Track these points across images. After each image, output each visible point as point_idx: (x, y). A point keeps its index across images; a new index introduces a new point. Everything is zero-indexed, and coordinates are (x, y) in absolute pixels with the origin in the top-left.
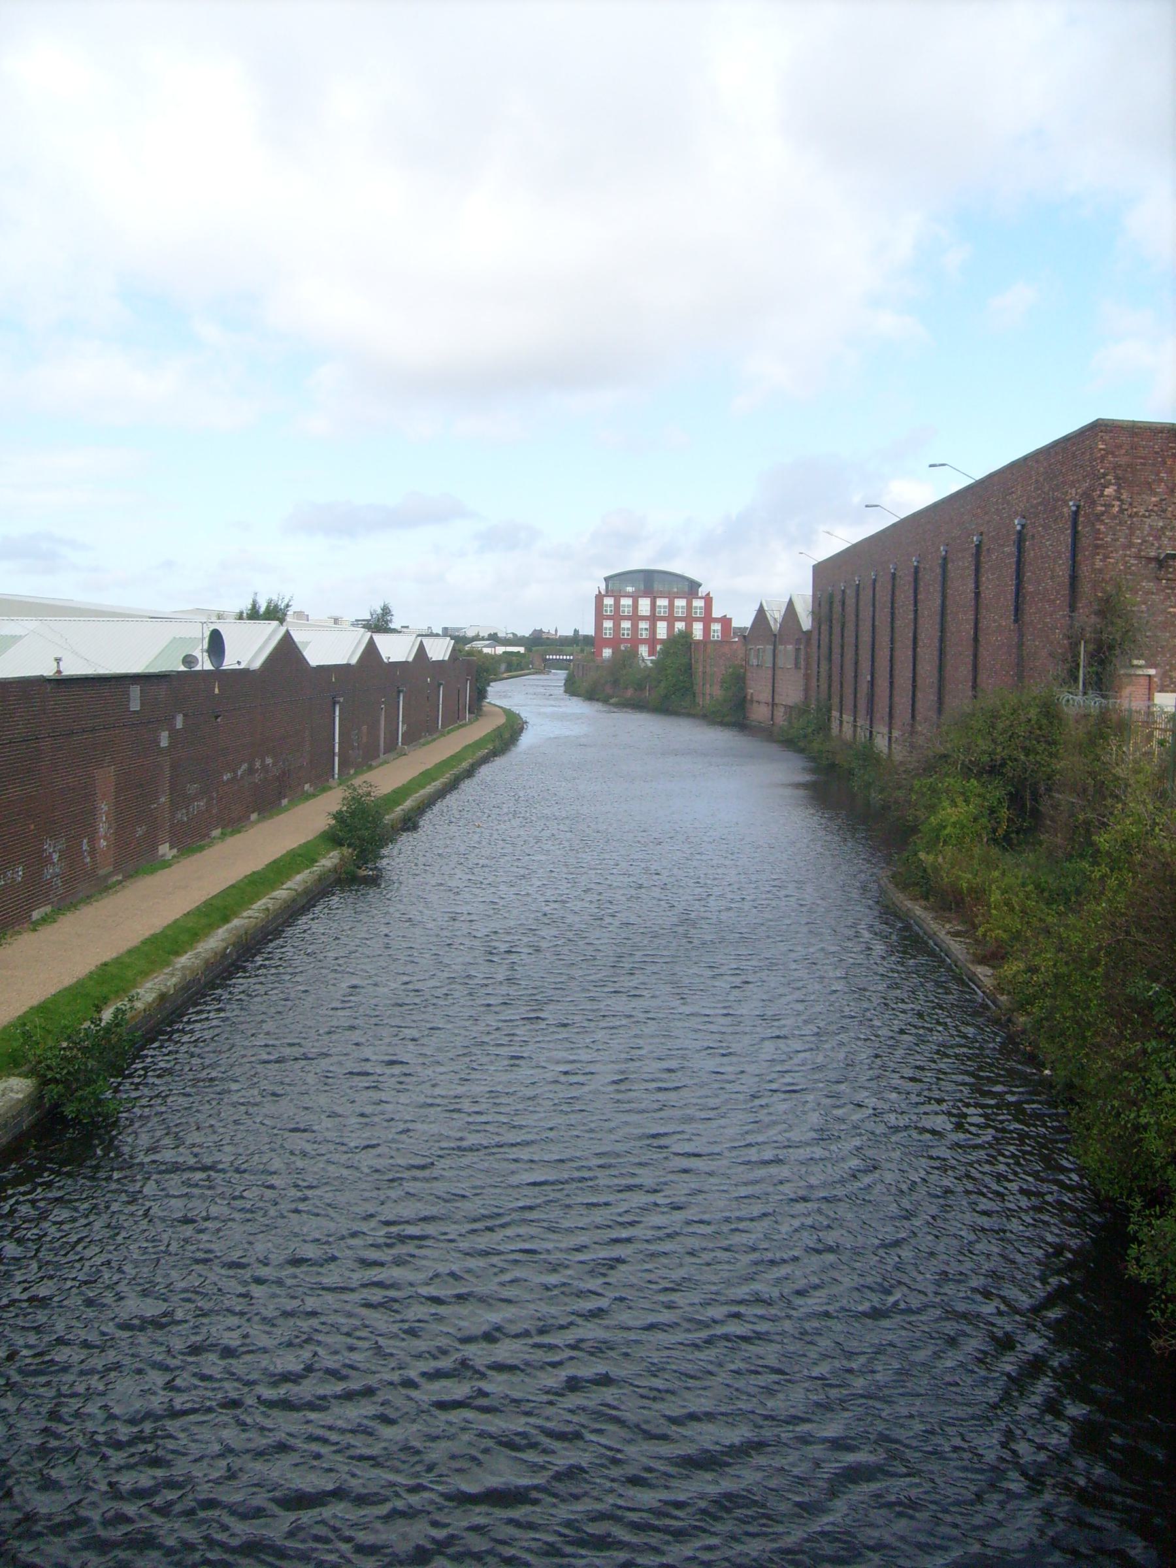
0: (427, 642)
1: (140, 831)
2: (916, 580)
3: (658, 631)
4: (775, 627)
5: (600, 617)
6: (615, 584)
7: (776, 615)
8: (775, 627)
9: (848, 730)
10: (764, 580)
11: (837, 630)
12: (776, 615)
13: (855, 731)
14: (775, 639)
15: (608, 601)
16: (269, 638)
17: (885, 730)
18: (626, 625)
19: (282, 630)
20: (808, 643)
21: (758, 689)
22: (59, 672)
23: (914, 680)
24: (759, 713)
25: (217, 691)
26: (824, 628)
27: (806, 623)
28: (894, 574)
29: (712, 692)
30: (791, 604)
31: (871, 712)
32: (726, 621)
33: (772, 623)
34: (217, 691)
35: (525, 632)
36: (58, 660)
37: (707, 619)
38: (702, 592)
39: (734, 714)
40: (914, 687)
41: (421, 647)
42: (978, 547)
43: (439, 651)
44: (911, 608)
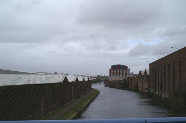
1: (47, 109)
4: (143, 74)
7: (143, 72)
8: (143, 74)
9: (157, 93)
10: (138, 66)
11: (154, 75)
12: (143, 72)
13: (158, 93)
14: (143, 76)
16: (63, 78)
17: (164, 92)
20: (149, 77)
21: (140, 85)
22: (29, 83)
24: (140, 89)
26: (152, 75)
27: (148, 74)
29: (133, 86)
30: (145, 70)
31: (161, 89)
33: (142, 74)
35: (96, 76)
36: (29, 81)
39: (136, 90)
41: (66, 78)
42: (180, 61)
43: (71, 79)
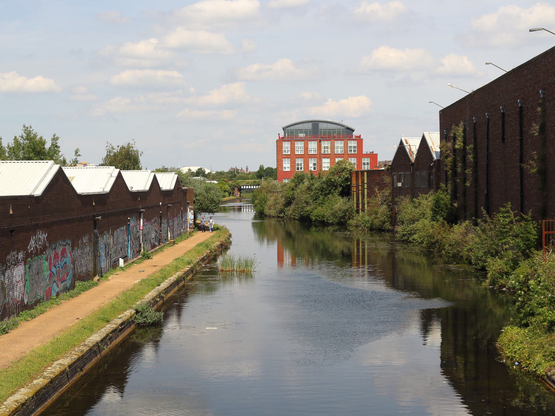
0: (159, 176)
2: (521, 116)
3: (324, 165)
5: (280, 156)
6: (290, 134)
15: (286, 146)
18: (300, 161)
19: (56, 167)
23: (522, 191)
25: (11, 212)
28: (503, 113)
32: (373, 156)
34: (11, 212)
37: (360, 155)
38: (355, 134)
40: (522, 197)
41: (155, 181)
43: (167, 182)
44: (518, 138)
